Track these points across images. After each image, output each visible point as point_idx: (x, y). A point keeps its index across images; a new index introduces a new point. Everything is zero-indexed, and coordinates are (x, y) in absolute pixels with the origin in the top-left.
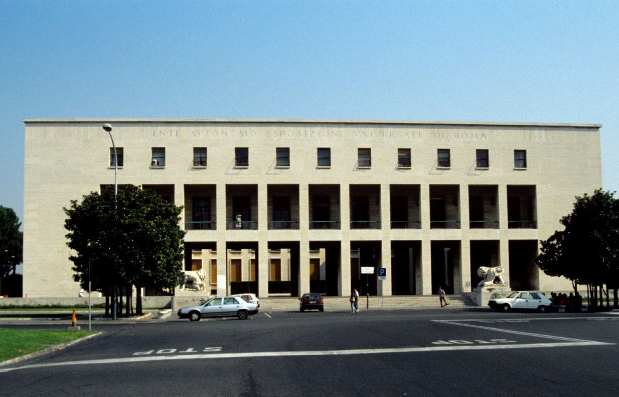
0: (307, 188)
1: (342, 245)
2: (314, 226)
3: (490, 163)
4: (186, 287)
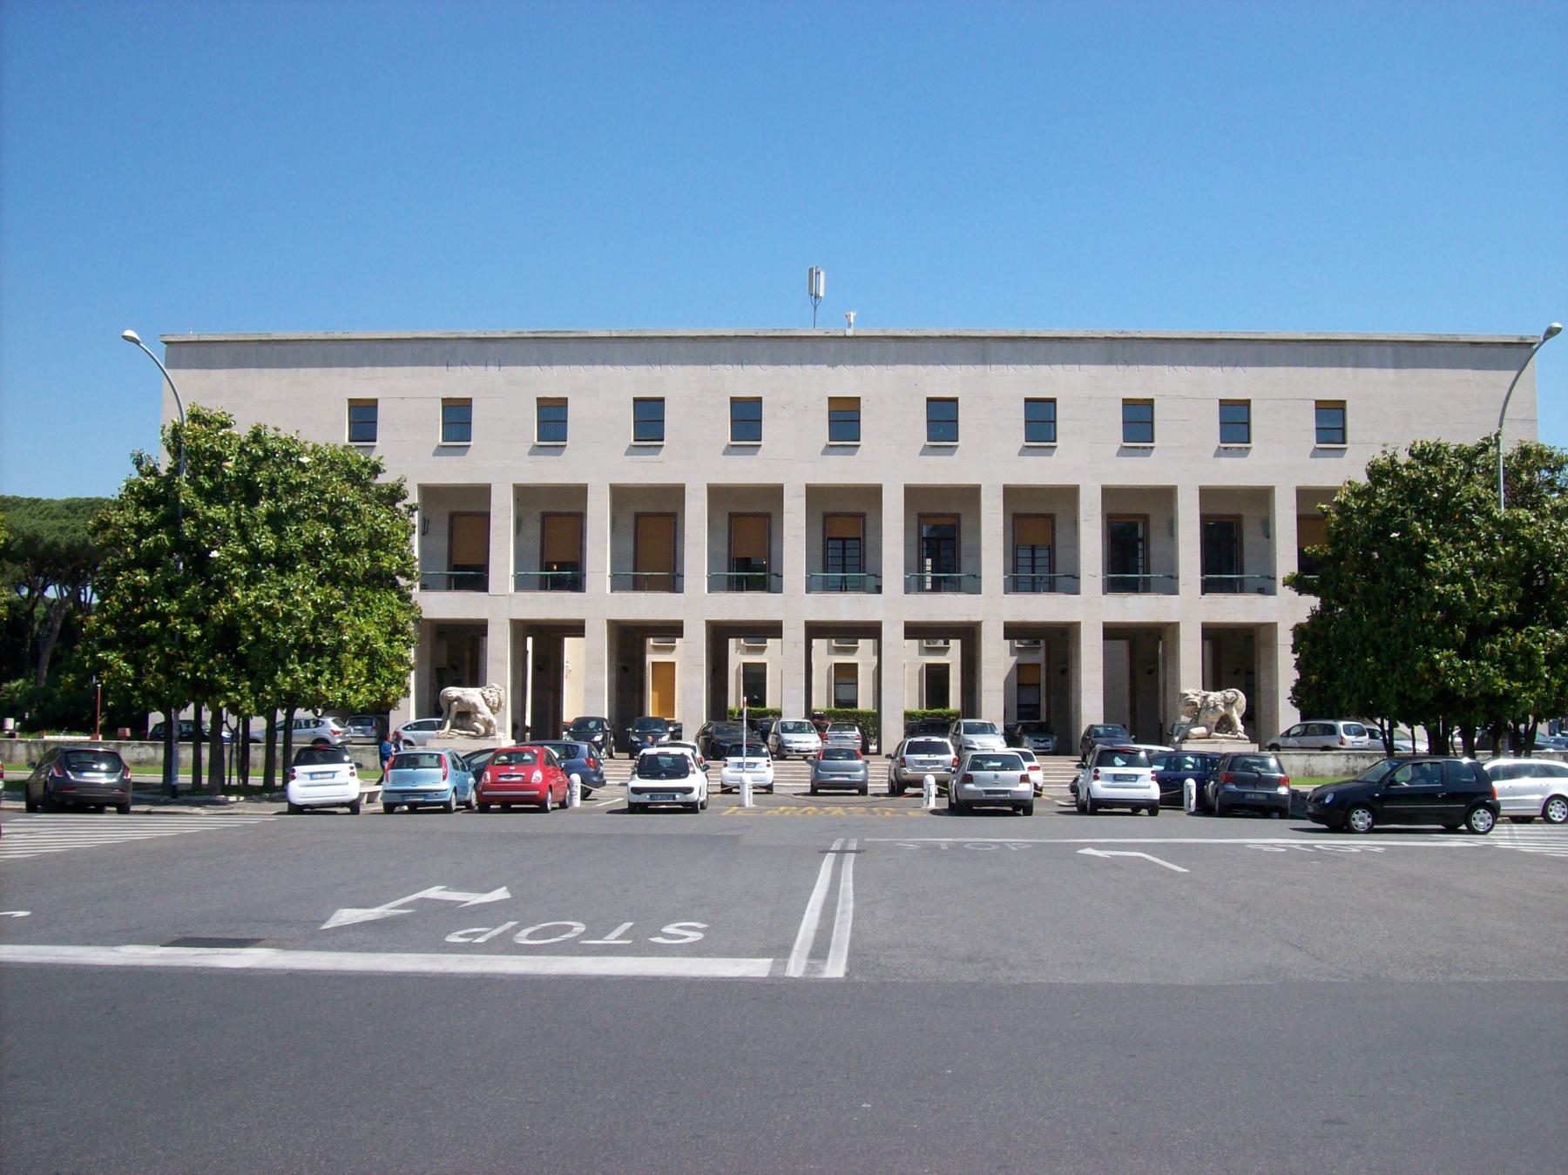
0: (803, 492)
1: (491, 630)
2: (1015, 585)
3: (1350, 435)
4: (453, 727)
